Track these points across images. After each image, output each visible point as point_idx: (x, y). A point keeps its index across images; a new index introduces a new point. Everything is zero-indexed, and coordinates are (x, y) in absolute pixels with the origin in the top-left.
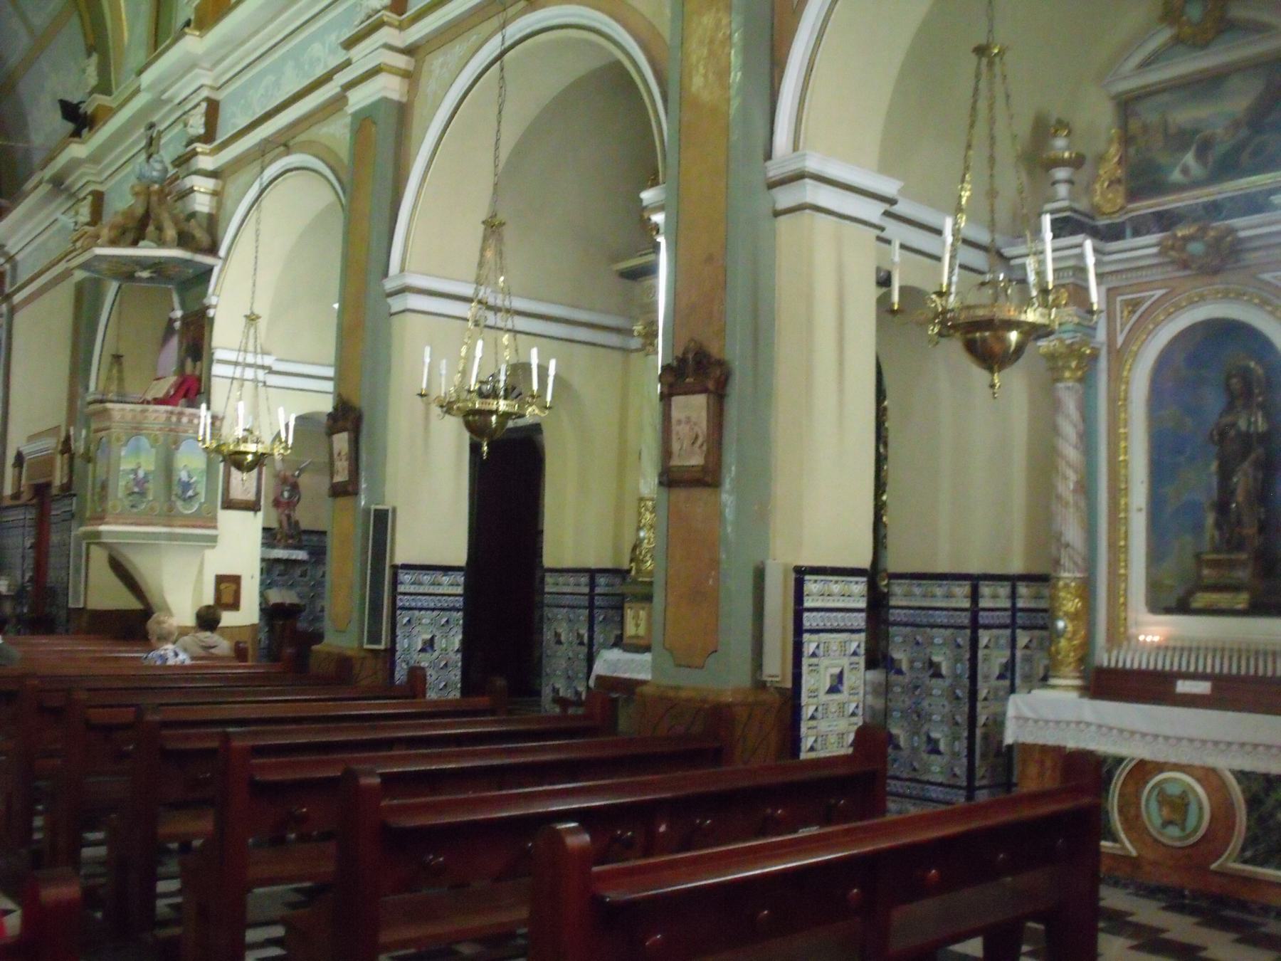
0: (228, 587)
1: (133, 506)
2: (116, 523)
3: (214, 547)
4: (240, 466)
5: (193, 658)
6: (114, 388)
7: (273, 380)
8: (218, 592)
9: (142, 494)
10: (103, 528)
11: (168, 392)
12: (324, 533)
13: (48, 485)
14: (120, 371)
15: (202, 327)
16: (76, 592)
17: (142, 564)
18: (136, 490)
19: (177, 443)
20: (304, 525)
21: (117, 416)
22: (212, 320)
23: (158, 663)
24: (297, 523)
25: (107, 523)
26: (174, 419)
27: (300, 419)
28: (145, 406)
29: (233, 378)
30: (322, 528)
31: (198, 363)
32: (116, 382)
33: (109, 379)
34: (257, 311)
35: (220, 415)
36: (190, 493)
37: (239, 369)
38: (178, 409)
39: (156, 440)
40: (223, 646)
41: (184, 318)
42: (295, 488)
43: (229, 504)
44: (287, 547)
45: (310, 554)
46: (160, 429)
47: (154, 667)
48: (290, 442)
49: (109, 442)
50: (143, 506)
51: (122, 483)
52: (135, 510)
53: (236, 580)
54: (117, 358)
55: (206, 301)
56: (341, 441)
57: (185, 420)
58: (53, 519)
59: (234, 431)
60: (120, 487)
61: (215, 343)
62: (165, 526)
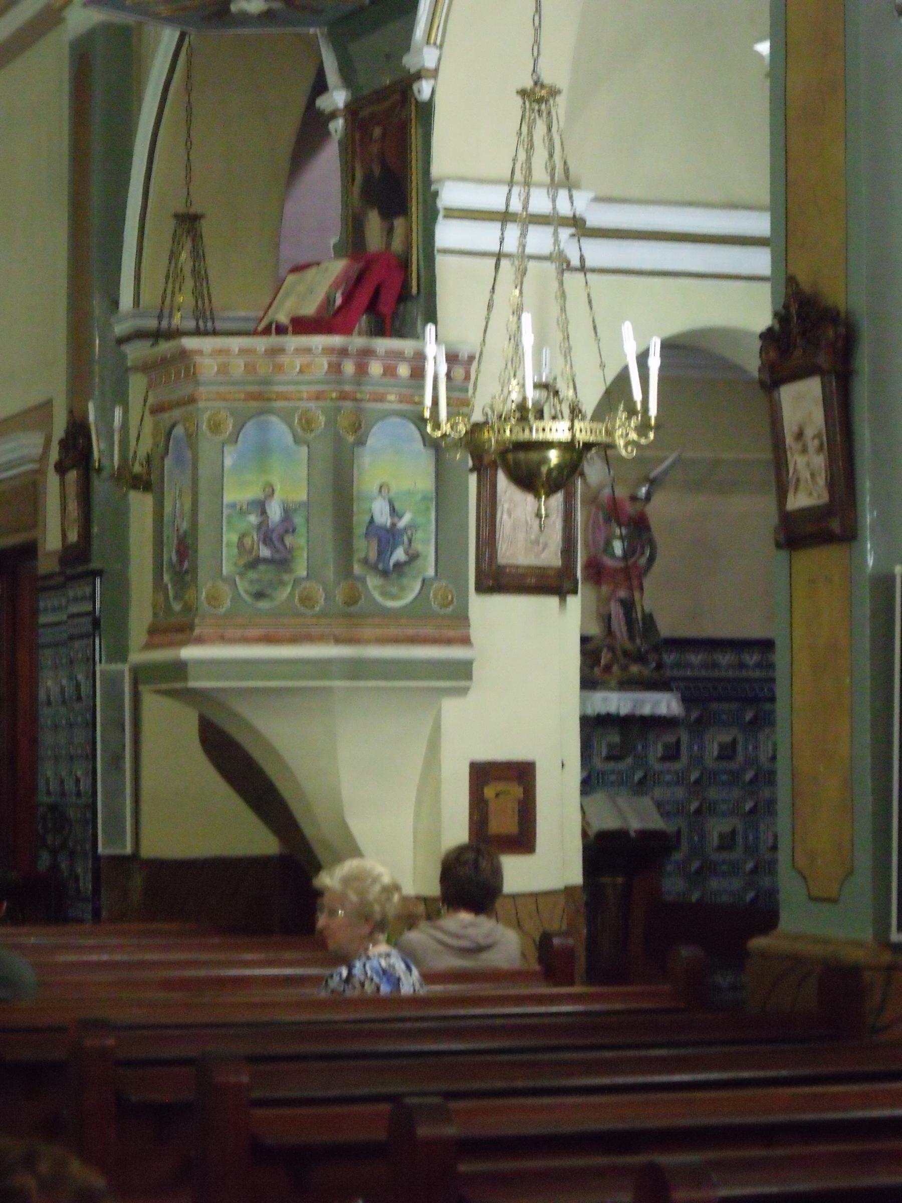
0: (501, 789)
1: (259, 595)
2: (223, 639)
3: (464, 691)
4: (527, 480)
5: (428, 977)
6: (184, 298)
7: (598, 253)
8: (478, 804)
9: (282, 562)
10: (189, 653)
11: (329, 300)
12: (766, 645)
13: (29, 550)
14: (198, 255)
15: (403, 129)
16: (115, 818)
17: (285, 739)
18: (265, 552)
19: (359, 430)
20: (666, 628)
21: (208, 367)
22: (427, 110)
23: (385, 989)
24: (649, 620)
25: (200, 641)
26: (349, 368)
27: (669, 347)
28: (274, 340)
29: (499, 256)
30: (756, 632)
31: (399, 223)
32: (189, 283)
33: (173, 276)
34: (547, 78)
35: (464, 354)
36: (399, 555)
37: (513, 231)
38: (357, 341)
39: (308, 423)
40: (506, 944)
41: (351, 111)
42: (639, 528)
43: (497, 580)
44: (627, 684)
45: (686, 700)
46: (318, 397)
47: (377, 1001)
48: (653, 411)
49: (192, 438)
50: (283, 594)
51: (230, 537)
52: (263, 605)
53: (522, 774)
54: (189, 222)
55: (410, 62)
56: (803, 403)
57: (376, 368)
58: (46, 636)
59: (497, 391)
60: (225, 549)
61: (437, 168)
62: (338, 640)
